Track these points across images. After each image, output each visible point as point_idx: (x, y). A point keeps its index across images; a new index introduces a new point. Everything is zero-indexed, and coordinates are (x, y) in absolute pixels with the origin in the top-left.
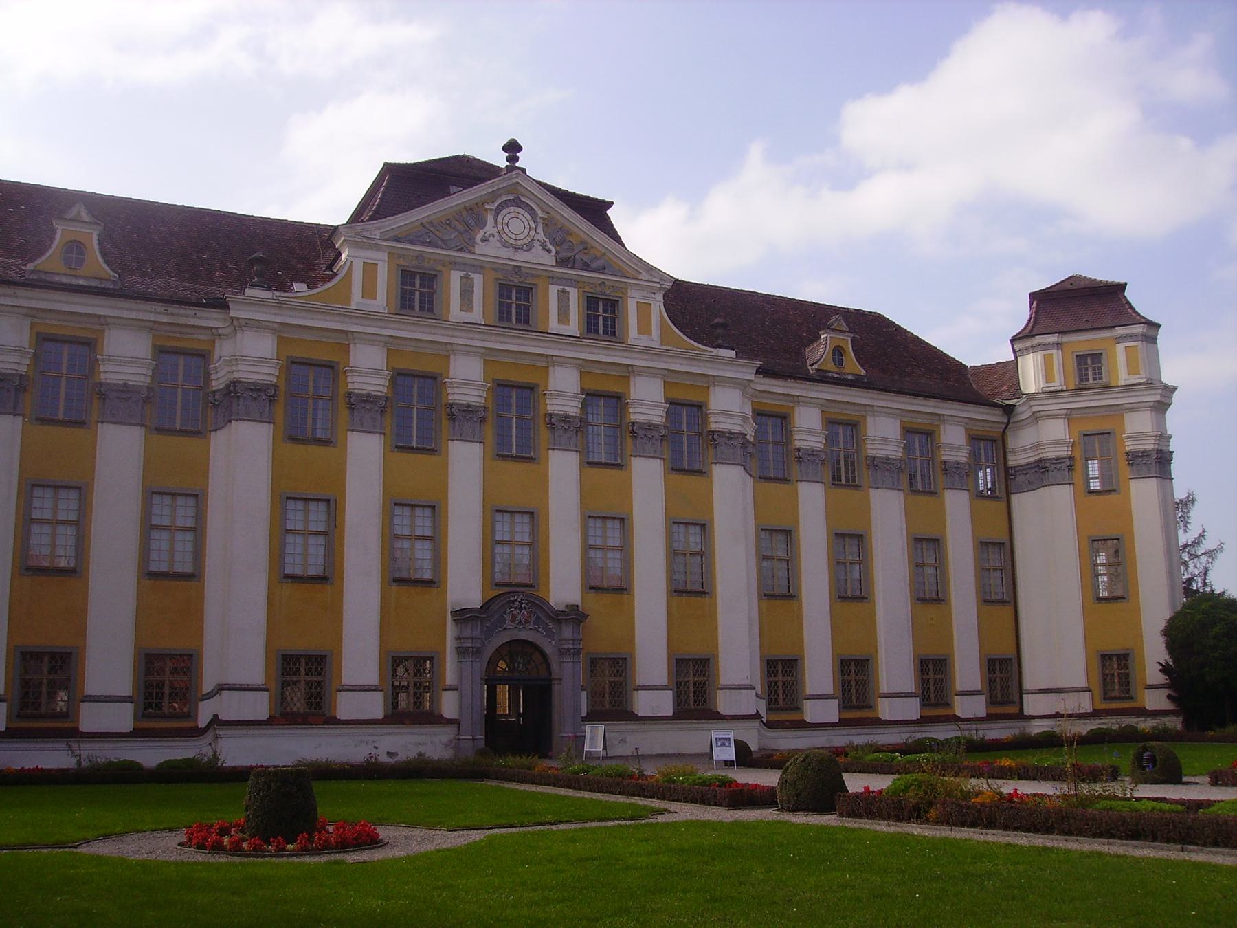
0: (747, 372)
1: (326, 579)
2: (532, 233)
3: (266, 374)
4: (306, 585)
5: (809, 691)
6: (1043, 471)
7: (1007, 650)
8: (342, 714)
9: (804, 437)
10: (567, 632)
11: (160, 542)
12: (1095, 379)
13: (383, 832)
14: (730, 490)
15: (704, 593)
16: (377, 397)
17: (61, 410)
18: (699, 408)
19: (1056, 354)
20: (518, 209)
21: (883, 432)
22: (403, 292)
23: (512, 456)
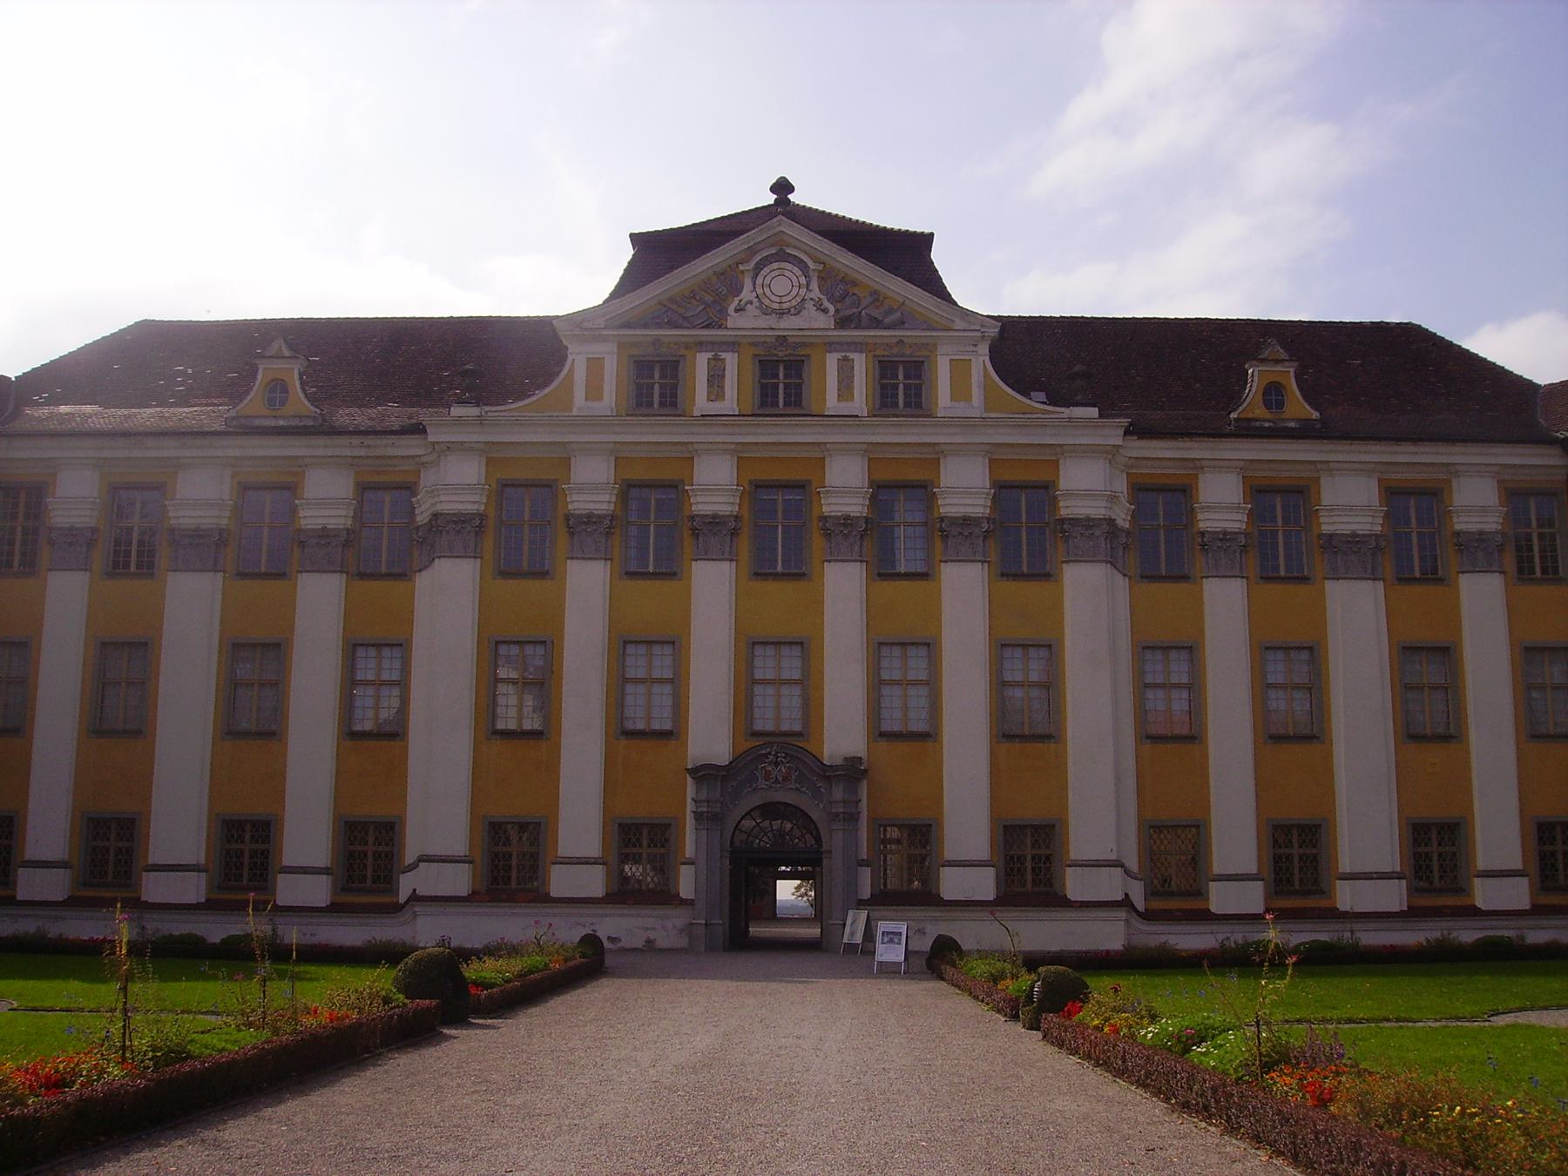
0: (1112, 434)
1: (540, 738)
4: (516, 745)
5: (564, 850)
8: (555, 892)
11: (892, 698)
14: (1091, 603)
16: (599, 516)
18: (1045, 489)
20: (783, 265)
23: (776, 575)
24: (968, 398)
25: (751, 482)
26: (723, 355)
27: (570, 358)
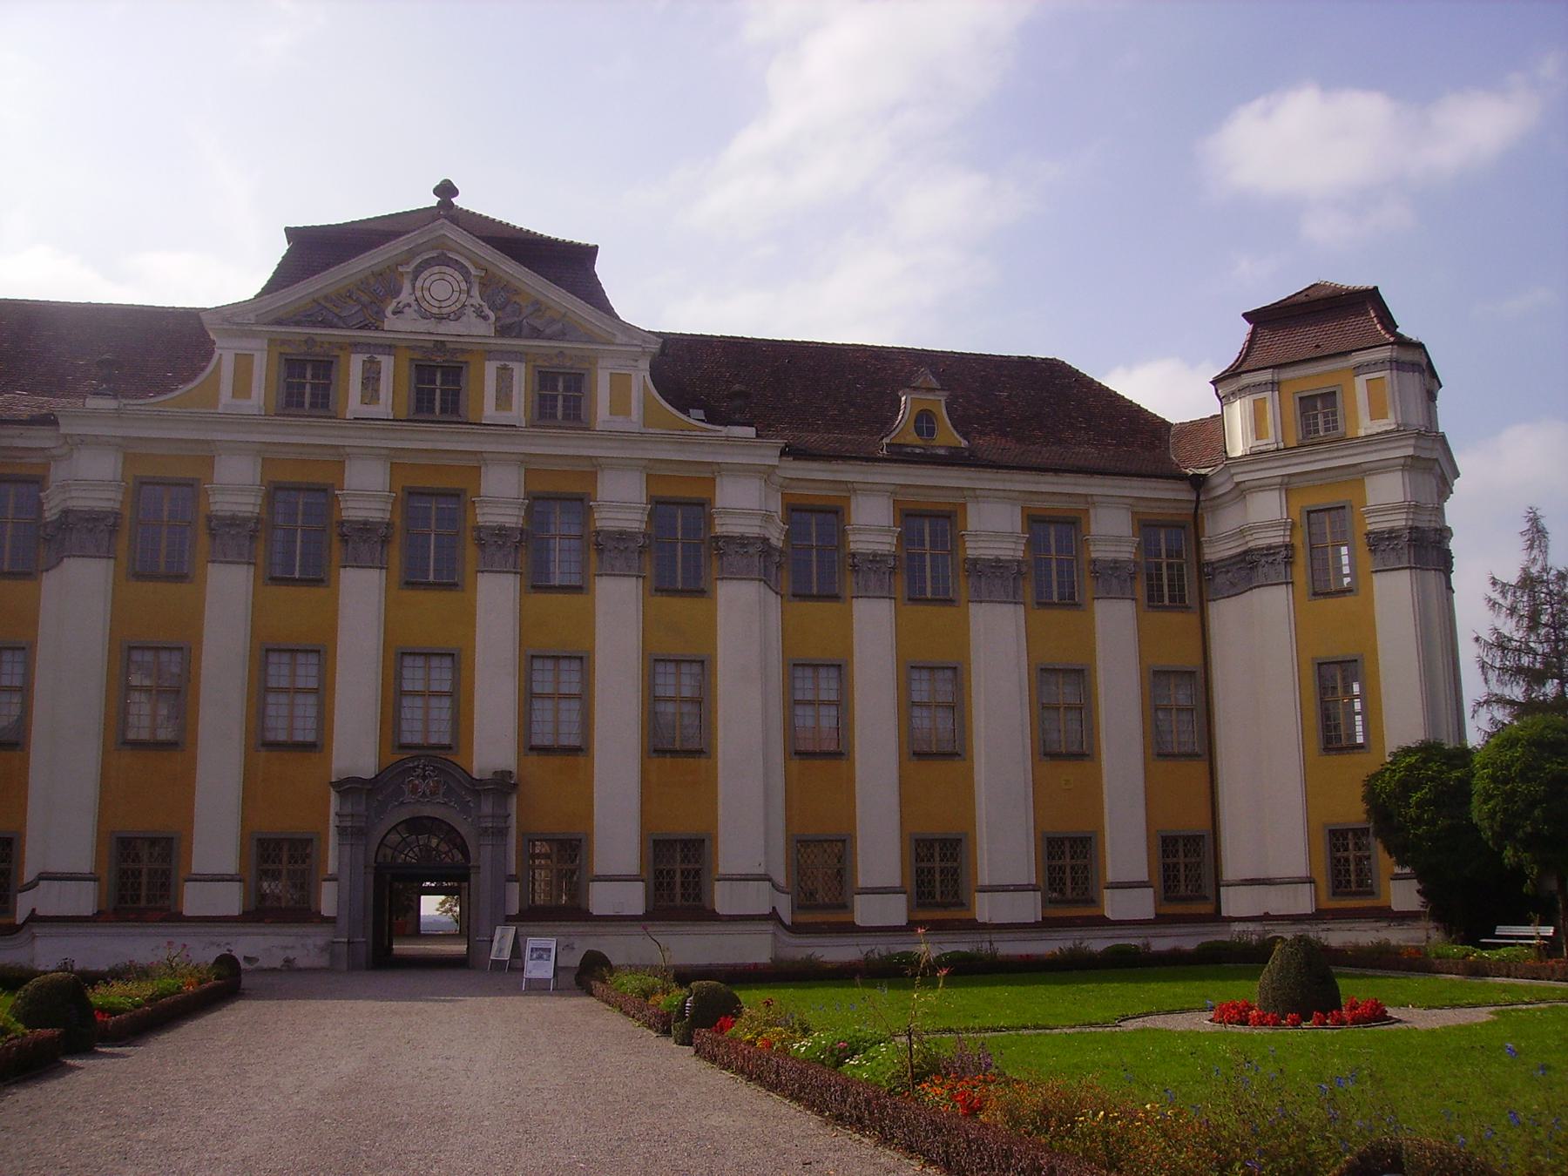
0: (768, 455)
1: (175, 747)
3: (103, 500)
6: (1249, 568)
7: (1195, 823)
8: (189, 909)
9: (863, 538)
11: (543, 712)
12: (1327, 430)
13: (1391, 1012)
16: (247, 520)
17: (929, 589)
18: (701, 507)
19: (1270, 398)
20: (444, 269)
21: (994, 523)
22: (542, 398)
26: (379, 358)
27: (217, 352)
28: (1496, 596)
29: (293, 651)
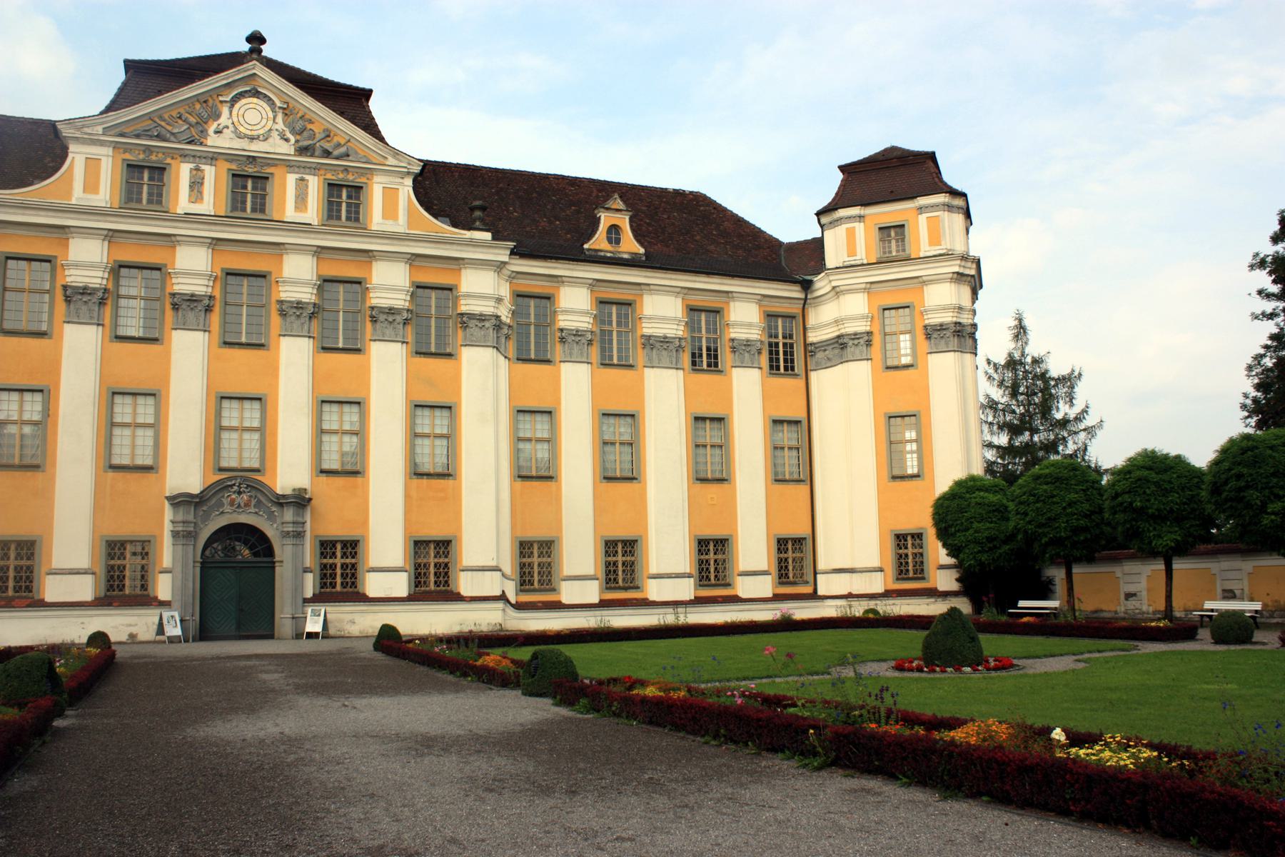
2: (270, 123)
5: (57, 563)
6: (842, 347)
8: (49, 597)
10: (289, 514)
11: (331, 443)
15: (449, 475)
16: (95, 289)
19: (859, 227)
24: (395, 218)
25: (222, 270)
26: (203, 167)
27: (70, 156)
28: (991, 371)
29: (135, 394)
